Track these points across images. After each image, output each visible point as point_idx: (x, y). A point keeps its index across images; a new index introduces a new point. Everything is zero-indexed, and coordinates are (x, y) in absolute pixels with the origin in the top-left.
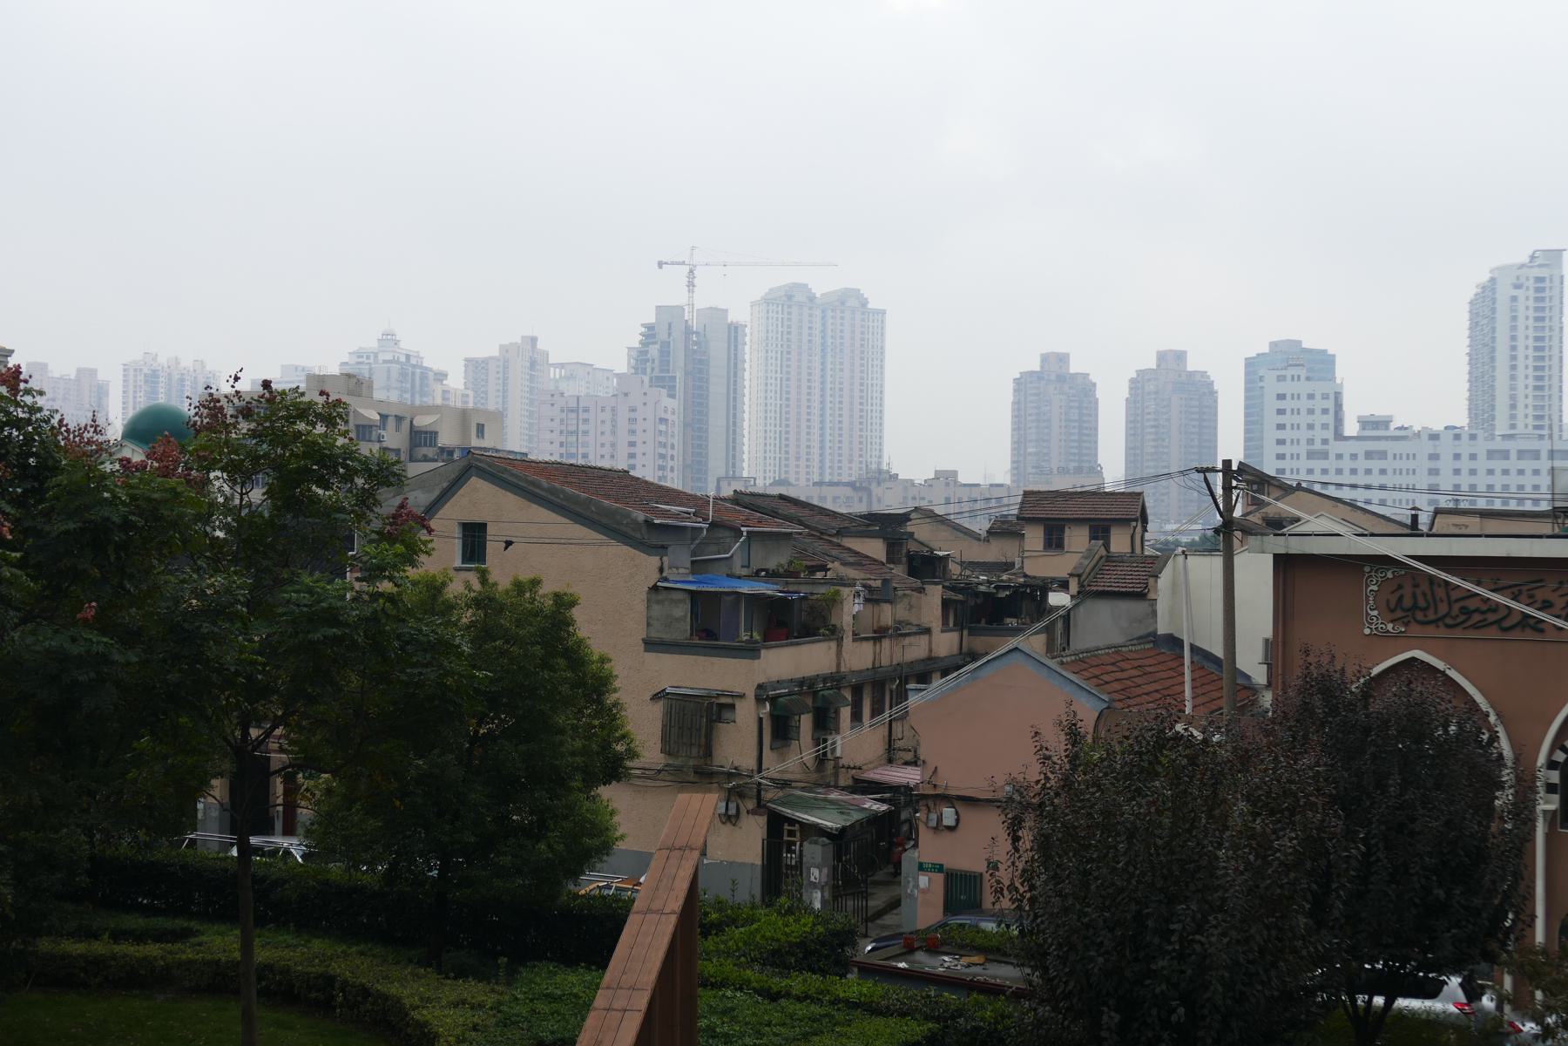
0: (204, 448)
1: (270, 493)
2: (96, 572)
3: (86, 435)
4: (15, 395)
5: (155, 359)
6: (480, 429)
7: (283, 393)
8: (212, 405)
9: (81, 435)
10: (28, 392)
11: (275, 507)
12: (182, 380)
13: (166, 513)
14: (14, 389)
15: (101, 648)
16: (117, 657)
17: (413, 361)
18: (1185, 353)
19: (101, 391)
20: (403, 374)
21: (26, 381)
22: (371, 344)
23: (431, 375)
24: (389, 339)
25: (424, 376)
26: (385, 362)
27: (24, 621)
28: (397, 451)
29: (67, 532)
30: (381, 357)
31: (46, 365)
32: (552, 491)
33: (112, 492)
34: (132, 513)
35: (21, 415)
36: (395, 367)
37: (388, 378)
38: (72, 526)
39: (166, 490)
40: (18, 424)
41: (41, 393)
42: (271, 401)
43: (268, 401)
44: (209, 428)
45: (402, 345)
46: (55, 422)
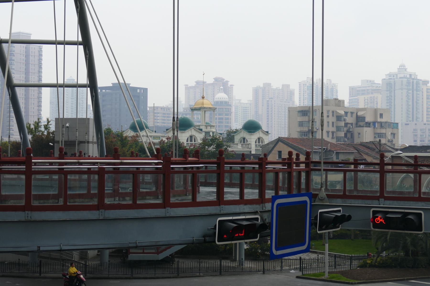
6: (381, 115)
17: (413, 77)
19: (292, 93)
20: (408, 83)
22: (395, 70)
23: (421, 82)
24: (402, 68)
25: (418, 83)
26: (400, 78)
28: (352, 124)
30: (399, 76)
32: (292, 144)
36: (405, 80)
37: (402, 84)
45: (408, 70)
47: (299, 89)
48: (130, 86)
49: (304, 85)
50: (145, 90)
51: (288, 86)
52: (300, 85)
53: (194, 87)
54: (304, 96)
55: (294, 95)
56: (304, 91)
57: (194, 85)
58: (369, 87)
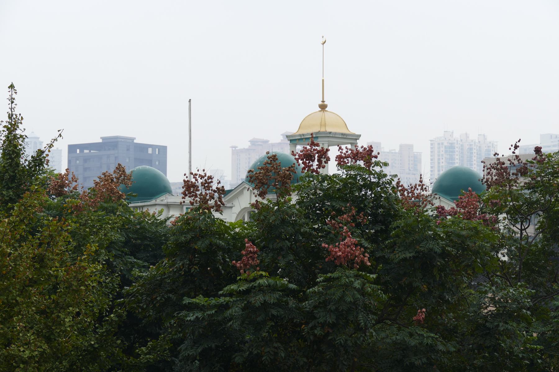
0: (494, 197)
1: (542, 228)
2: (425, 288)
3: (416, 191)
4: (369, 167)
5: (452, 135)
7: (549, 156)
8: (499, 167)
9: (412, 192)
10: (377, 164)
11: (545, 238)
12: (471, 149)
13: (471, 245)
14: (368, 163)
15: (430, 342)
16: (441, 348)
18: (166, 147)
19: (416, 160)
21: (376, 157)
27: (378, 322)
29: (405, 259)
31: (380, 144)
33: (434, 231)
34: (446, 246)
35: (373, 180)
38: (408, 255)
39: (470, 229)
40: (370, 186)
41: (386, 164)
42: (541, 162)
43: (539, 161)
44: (497, 183)
46: (394, 183)
47: (431, 152)
48: (135, 141)
49: (439, 144)
50: (163, 150)
51: (410, 147)
52: (432, 144)
53: (248, 150)
54: (439, 163)
55: (420, 162)
56: (439, 156)
57: (247, 147)
58: (554, 146)
